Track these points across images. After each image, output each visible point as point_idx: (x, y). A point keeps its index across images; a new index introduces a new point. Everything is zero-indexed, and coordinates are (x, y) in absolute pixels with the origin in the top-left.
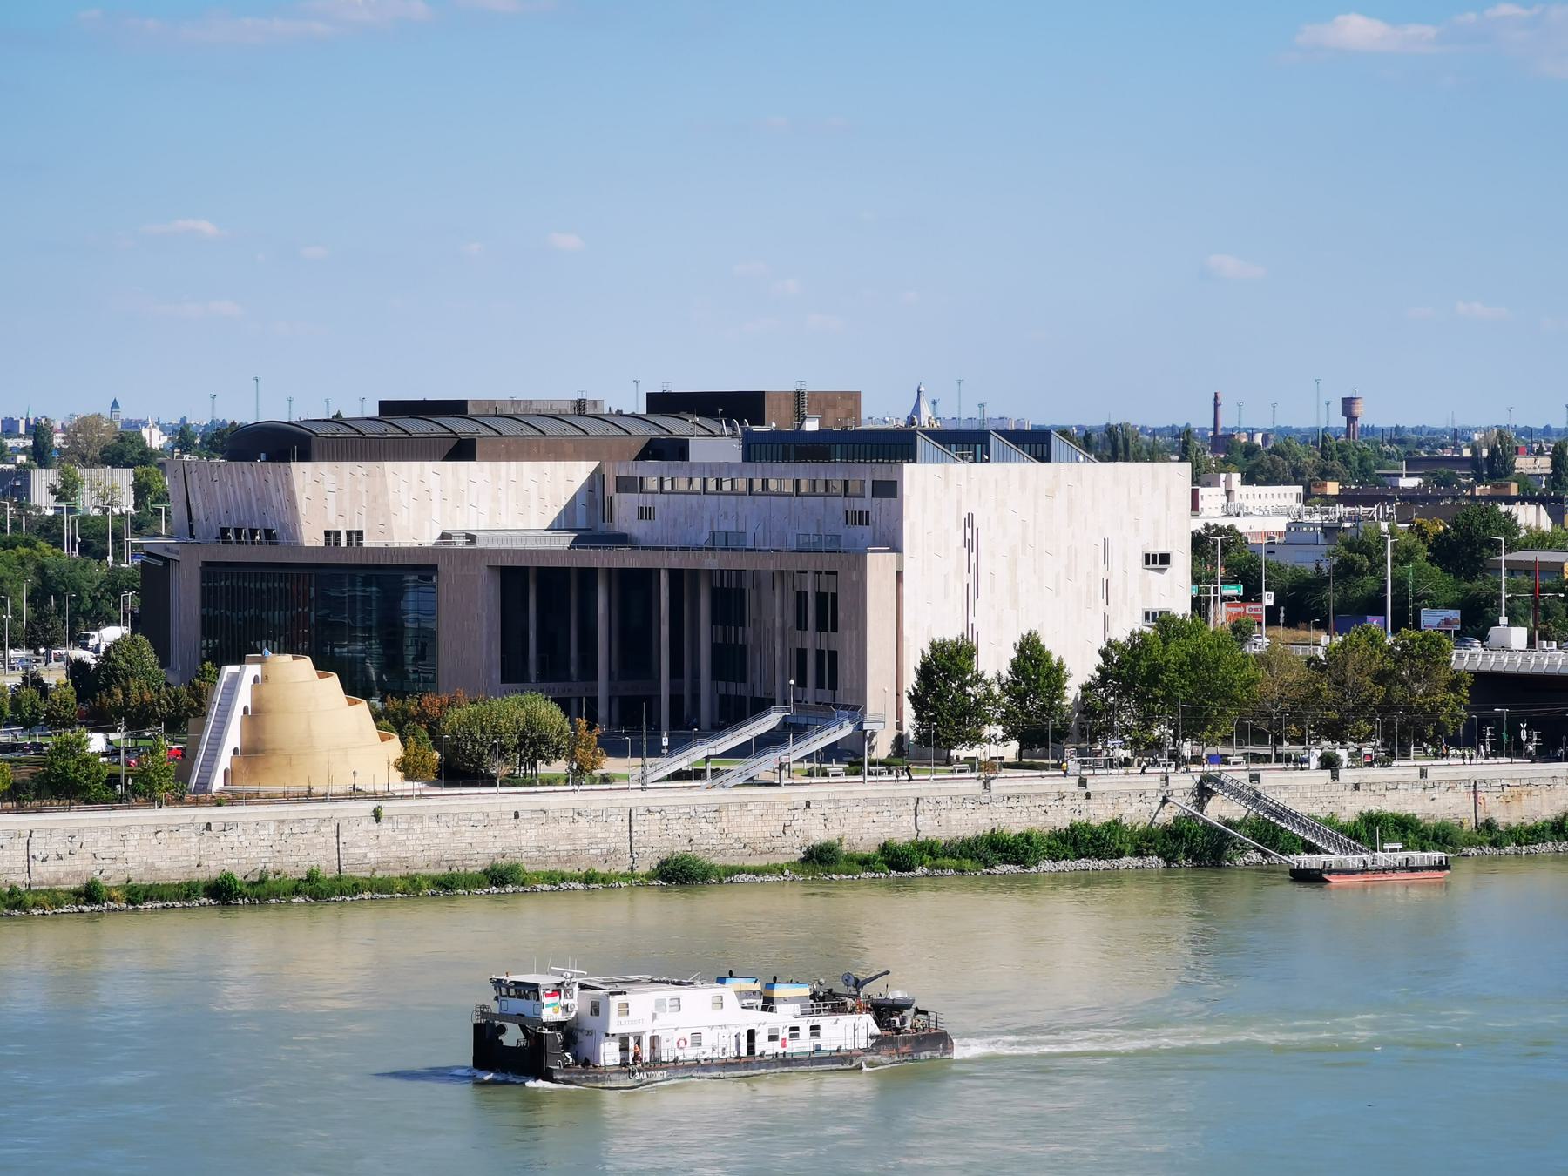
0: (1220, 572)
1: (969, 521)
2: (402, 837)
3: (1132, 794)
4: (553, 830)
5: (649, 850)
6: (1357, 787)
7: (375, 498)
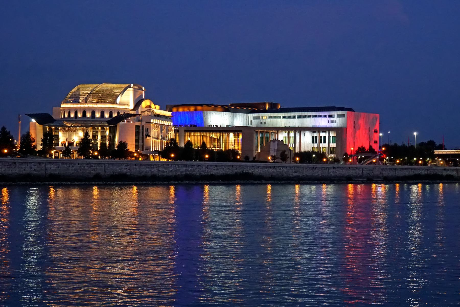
1: (354, 123)
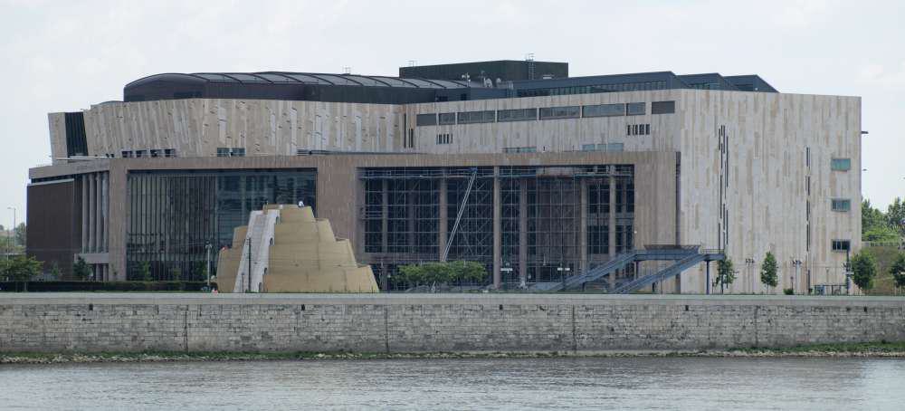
1: (722, 131)
2: (427, 321)
3: (591, 353)
4: (525, 320)
5: (586, 337)
7: (253, 126)
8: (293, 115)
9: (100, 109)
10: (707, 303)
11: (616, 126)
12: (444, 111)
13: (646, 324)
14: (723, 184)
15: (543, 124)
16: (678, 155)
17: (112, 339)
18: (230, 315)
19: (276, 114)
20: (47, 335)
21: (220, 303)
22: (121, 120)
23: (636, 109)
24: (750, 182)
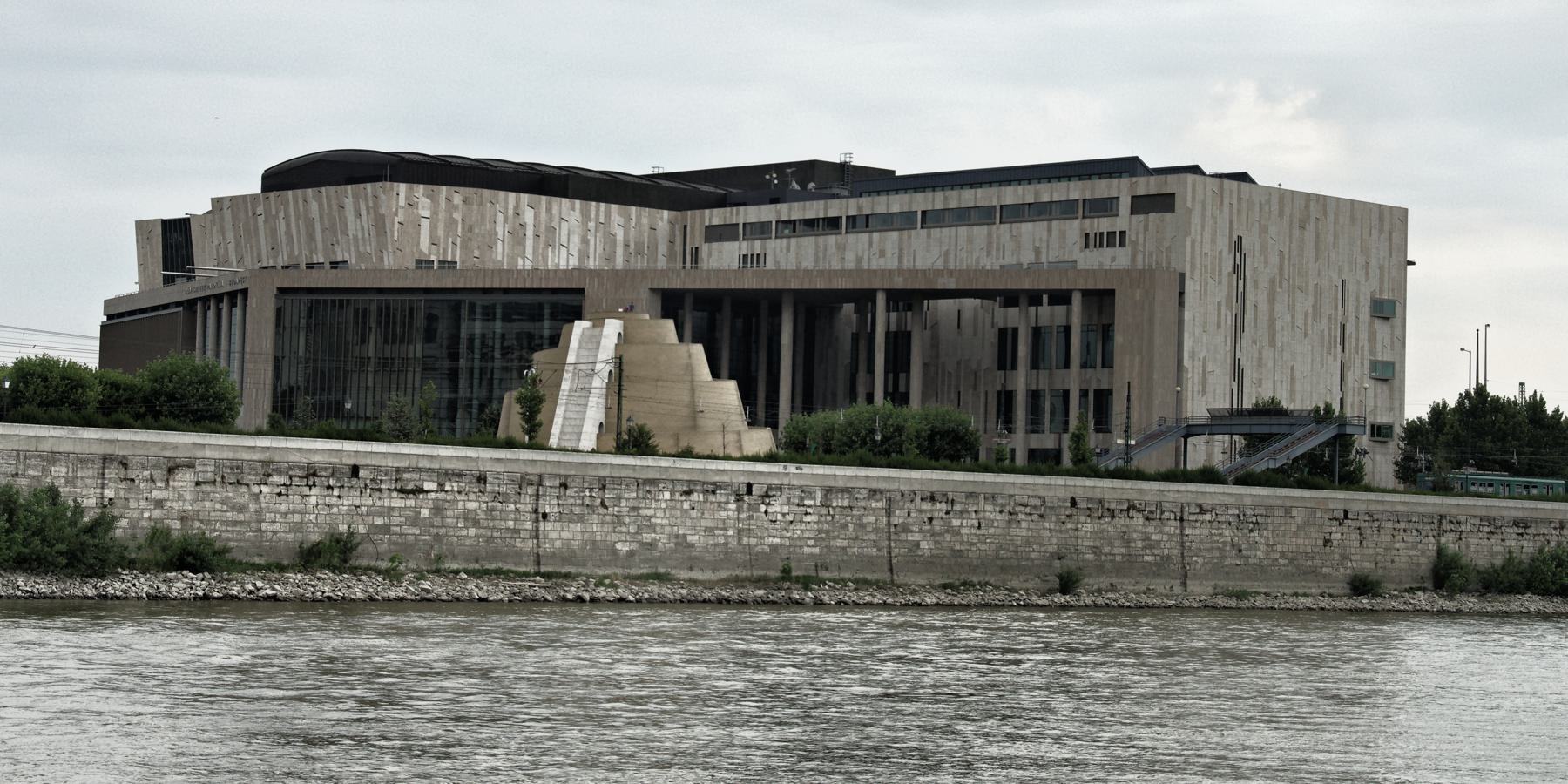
0: (109, 493)
1: (1238, 246)
2: (956, 523)
5: (1200, 560)
6: (1327, 542)
7: (471, 229)
8: (529, 216)
9: (227, 204)
10: (1372, 508)
11: (1063, 235)
12: (752, 219)
13: (1287, 541)
14: (1238, 329)
15: (929, 236)
16: (1182, 276)
17: (394, 538)
18: (619, 499)
19: (505, 214)
20: (264, 526)
21: (602, 473)
22: (261, 220)
23: (1105, 206)
24: (1272, 322)
